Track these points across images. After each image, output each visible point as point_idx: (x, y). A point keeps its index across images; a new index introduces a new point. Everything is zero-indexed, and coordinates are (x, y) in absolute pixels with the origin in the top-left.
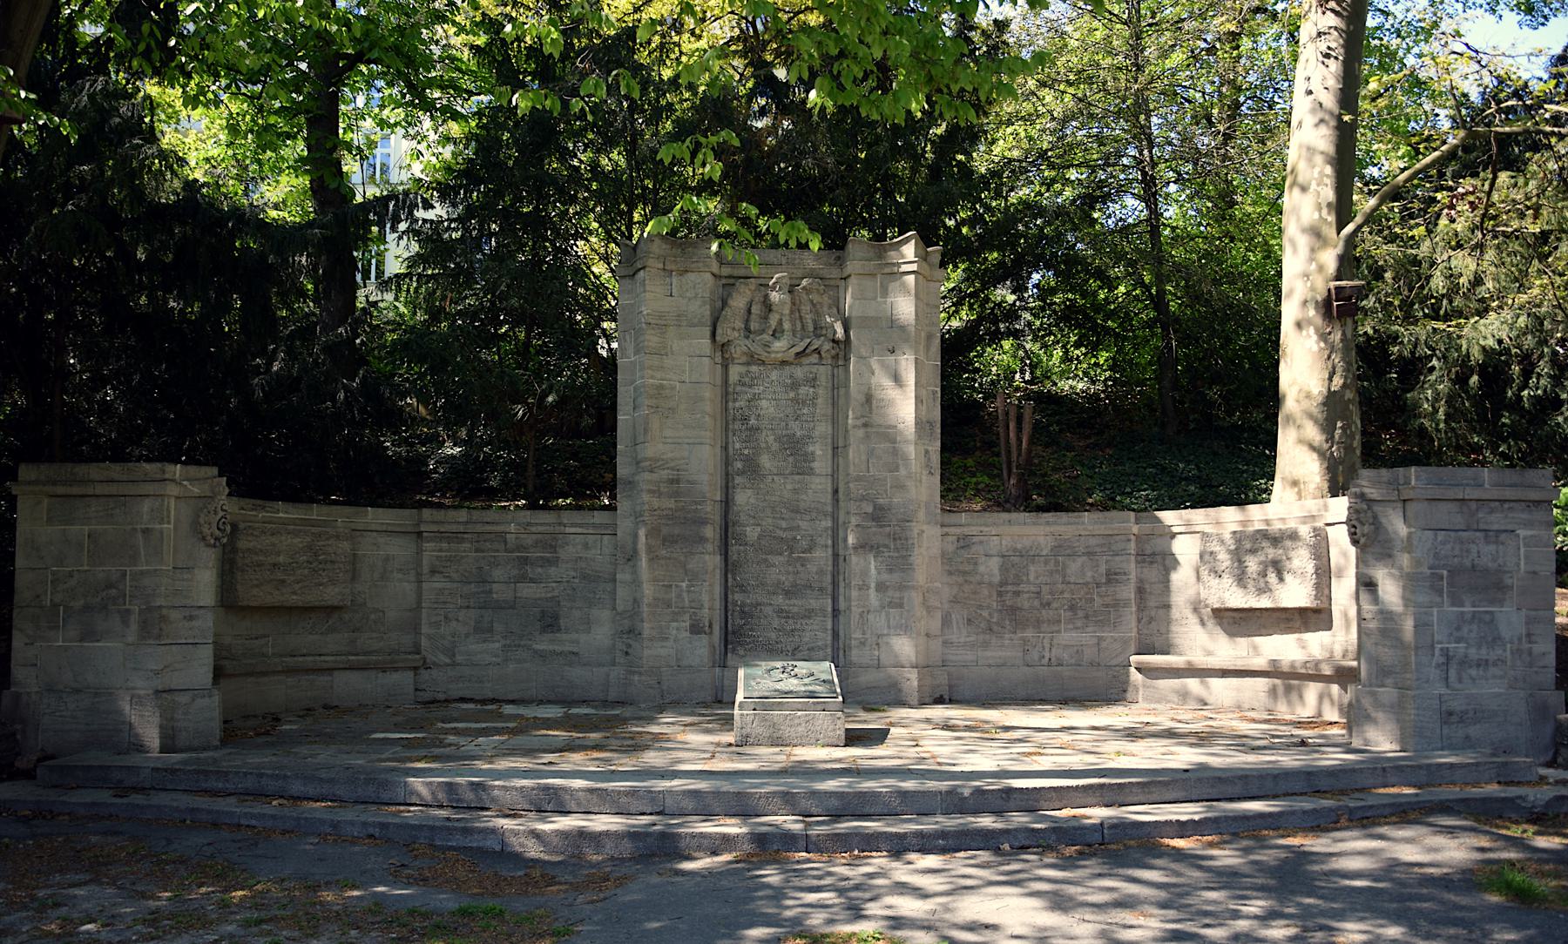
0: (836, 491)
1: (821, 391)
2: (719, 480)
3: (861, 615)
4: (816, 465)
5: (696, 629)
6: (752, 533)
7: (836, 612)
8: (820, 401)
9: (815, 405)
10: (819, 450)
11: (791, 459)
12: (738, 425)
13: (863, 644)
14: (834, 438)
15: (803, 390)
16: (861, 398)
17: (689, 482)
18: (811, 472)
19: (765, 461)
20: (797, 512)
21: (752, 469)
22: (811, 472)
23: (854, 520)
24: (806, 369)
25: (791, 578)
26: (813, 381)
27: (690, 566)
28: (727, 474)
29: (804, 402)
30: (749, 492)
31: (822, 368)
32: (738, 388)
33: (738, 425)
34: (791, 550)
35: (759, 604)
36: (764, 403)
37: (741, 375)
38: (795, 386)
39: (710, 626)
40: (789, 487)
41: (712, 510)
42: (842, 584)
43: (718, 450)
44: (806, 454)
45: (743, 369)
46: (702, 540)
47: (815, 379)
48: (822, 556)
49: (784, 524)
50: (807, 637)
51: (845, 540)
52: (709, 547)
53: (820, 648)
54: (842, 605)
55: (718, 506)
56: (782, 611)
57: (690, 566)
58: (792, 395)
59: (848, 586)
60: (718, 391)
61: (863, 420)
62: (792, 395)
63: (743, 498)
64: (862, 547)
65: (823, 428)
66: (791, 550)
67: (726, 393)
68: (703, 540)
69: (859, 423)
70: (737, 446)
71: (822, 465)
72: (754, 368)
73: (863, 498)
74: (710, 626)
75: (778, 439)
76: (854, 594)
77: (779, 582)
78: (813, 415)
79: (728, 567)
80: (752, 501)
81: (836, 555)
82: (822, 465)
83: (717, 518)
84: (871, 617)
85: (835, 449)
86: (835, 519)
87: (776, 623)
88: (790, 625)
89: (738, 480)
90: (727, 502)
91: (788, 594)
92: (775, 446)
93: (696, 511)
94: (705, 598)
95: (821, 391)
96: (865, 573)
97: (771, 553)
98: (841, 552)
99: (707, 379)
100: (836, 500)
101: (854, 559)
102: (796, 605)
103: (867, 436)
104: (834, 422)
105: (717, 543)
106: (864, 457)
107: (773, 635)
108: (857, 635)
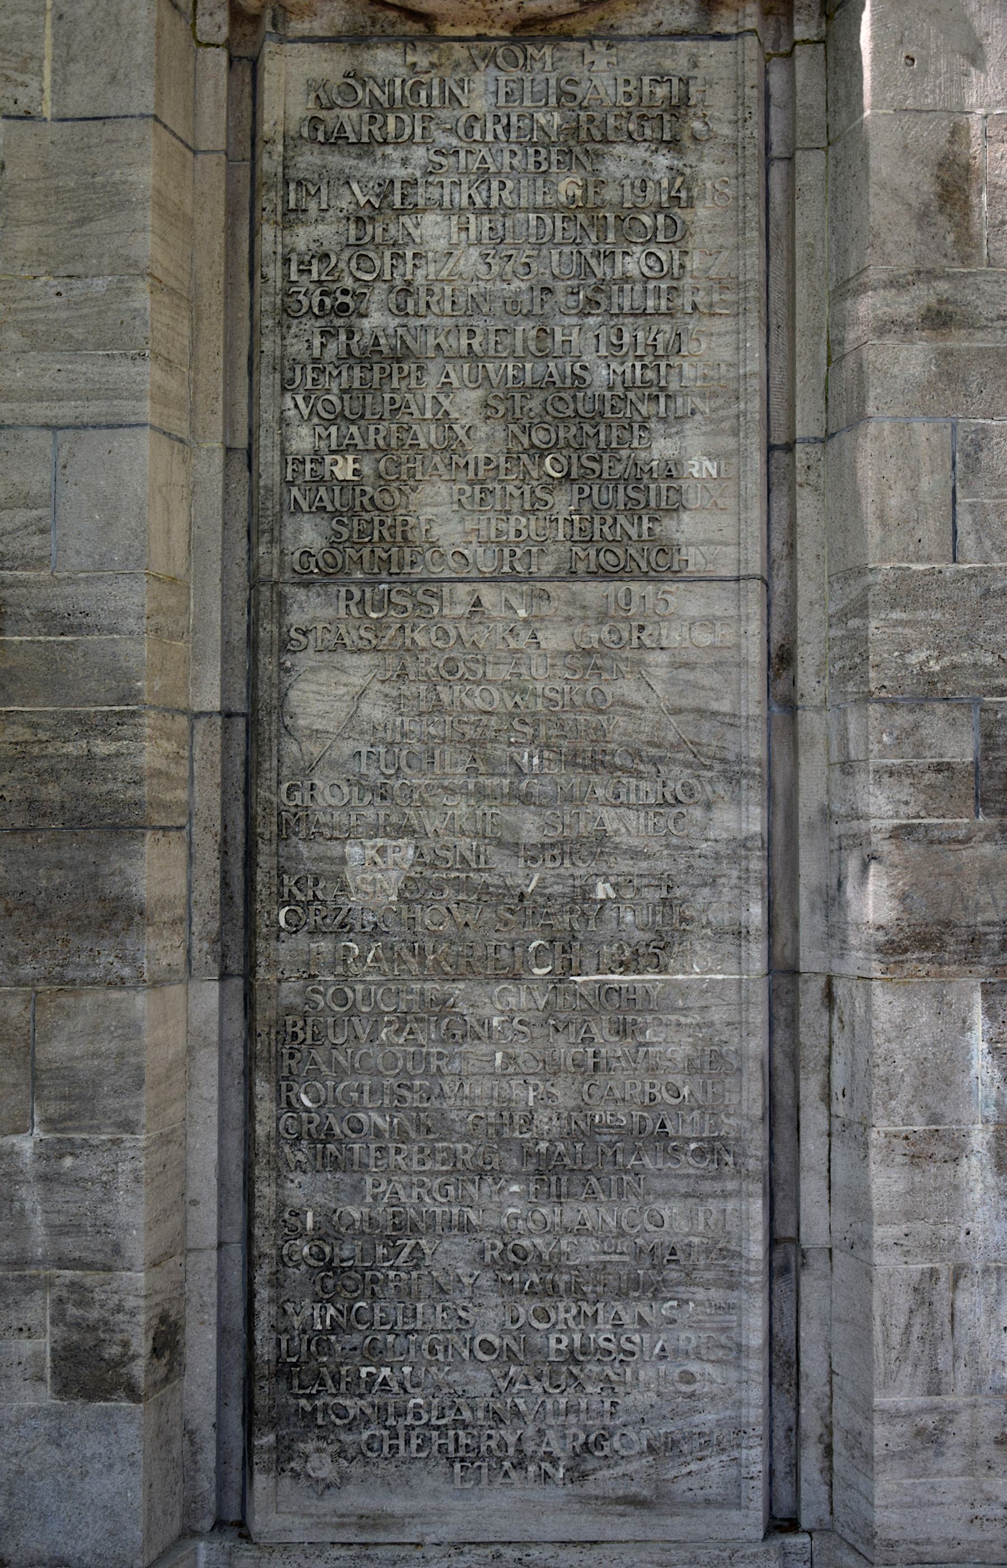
0: (781, 660)
1: (709, 167)
2: (211, 610)
3: (922, 1292)
4: (686, 528)
5: (85, 1371)
6: (373, 871)
7: (785, 1255)
8: (703, 213)
9: (677, 233)
10: (702, 457)
11: (563, 502)
12: (303, 340)
13: (930, 1439)
14: (778, 394)
15: (622, 162)
16: (921, 183)
17: (52, 620)
18: (662, 565)
19: (440, 513)
20: (597, 763)
21: (372, 553)
22: (662, 565)
23: (881, 806)
24: (636, 58)
25: (564, 1094)
26: (667, 122)
27: (55, 1050)
28: (254, 582)
29: (626, 219)
30: (359, 670)
31: (714, 56)
32: (309, 160)
33: (303, 340)
34: (566, 950)
35: (403, 1227)
36: (432, 229)
37: (317, 89)
38: (582, 141)
39: (167, 1340)
40: (555, 639)
41: (170, 762)
42: (814, 1119)
43: (210, 465)
44: (636, 477)
45: (328, 65)
46: (120, 915)
47: (678, 107)
48: (715, 981)
49: (530, 826)
50: (645, 1386)
51: (833, 899)
52: (160, 949)
53: (707, 1442)
54: (816, 1221)
55: (208, 740)
56: (519, 1258)
57: (55, 1050)
58: (567, 185)
59: (853, 1132)
60: (212, 175)
61: (925, 295)
62: (567, 185)
63: (329, 697)
64: (922, 941)
65: (718, 350)
66: (566, 950)
67: (255, 187)
68: (121, 915)
69: (906, 305)
70: (303, 440)
71: (714, 525)
72: (385, 61)
73: (928, 692)
74: (167, 1340)
75: (504, 404)
76: (886, 1182)
77: (506, 1114)
78: (673, 277)
79: (265, 1045)
80: (374, 711)
81: (784, 974)
82: (714, 525)
83: (208, 797)
84: (970, 1300)
85: (779, 449)
86: (781, 800)
87: (490, 1320)
88: (560, 1330)
89: (308, 609)
90: (253, 722)
91: (551, 1173)
92: (487, 439)
93: (86, 766)
94: (132, 1214)
95: (709, 167)
96: (941, 1073)
97: (467, 968)
98: (811, 960)
99: (143, 97)
100: (785, 706)
101: (886, 1005)
102: (588, 1228)
103: (949, 372)
104: (777, 323)
105: (206, 920)
106: (931, 484)
107: (478, 1381)
108: (899, 1395)
